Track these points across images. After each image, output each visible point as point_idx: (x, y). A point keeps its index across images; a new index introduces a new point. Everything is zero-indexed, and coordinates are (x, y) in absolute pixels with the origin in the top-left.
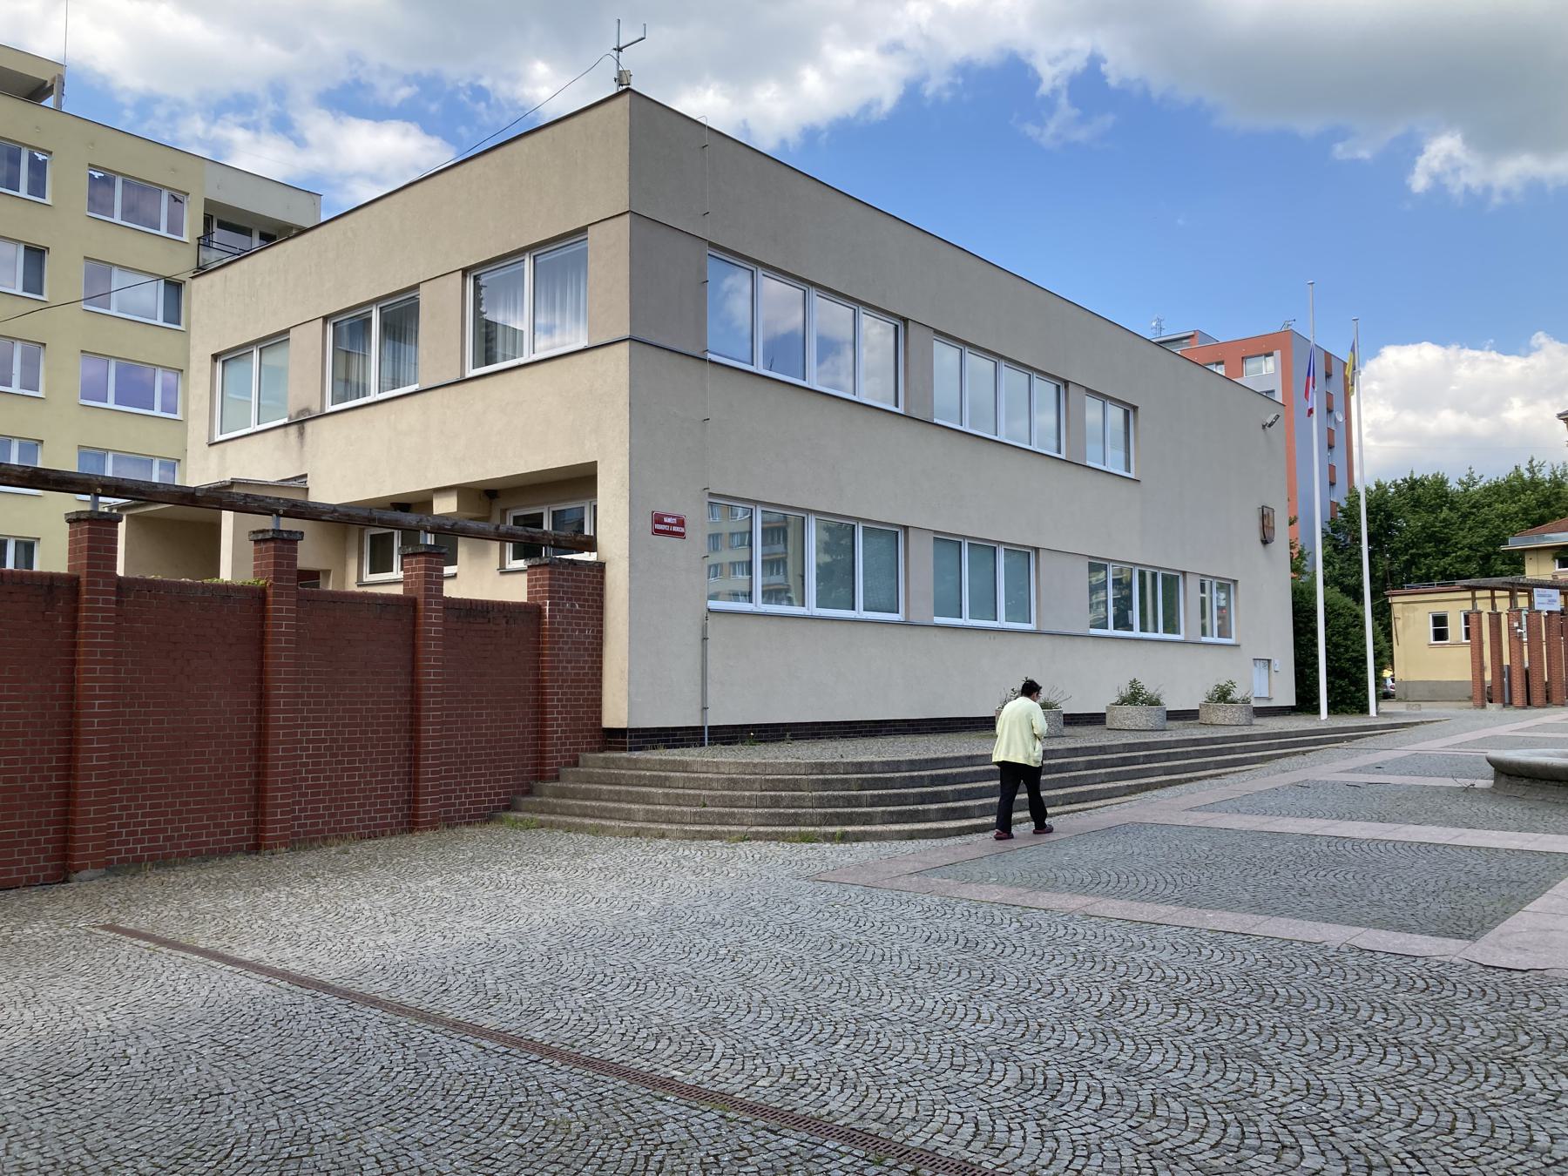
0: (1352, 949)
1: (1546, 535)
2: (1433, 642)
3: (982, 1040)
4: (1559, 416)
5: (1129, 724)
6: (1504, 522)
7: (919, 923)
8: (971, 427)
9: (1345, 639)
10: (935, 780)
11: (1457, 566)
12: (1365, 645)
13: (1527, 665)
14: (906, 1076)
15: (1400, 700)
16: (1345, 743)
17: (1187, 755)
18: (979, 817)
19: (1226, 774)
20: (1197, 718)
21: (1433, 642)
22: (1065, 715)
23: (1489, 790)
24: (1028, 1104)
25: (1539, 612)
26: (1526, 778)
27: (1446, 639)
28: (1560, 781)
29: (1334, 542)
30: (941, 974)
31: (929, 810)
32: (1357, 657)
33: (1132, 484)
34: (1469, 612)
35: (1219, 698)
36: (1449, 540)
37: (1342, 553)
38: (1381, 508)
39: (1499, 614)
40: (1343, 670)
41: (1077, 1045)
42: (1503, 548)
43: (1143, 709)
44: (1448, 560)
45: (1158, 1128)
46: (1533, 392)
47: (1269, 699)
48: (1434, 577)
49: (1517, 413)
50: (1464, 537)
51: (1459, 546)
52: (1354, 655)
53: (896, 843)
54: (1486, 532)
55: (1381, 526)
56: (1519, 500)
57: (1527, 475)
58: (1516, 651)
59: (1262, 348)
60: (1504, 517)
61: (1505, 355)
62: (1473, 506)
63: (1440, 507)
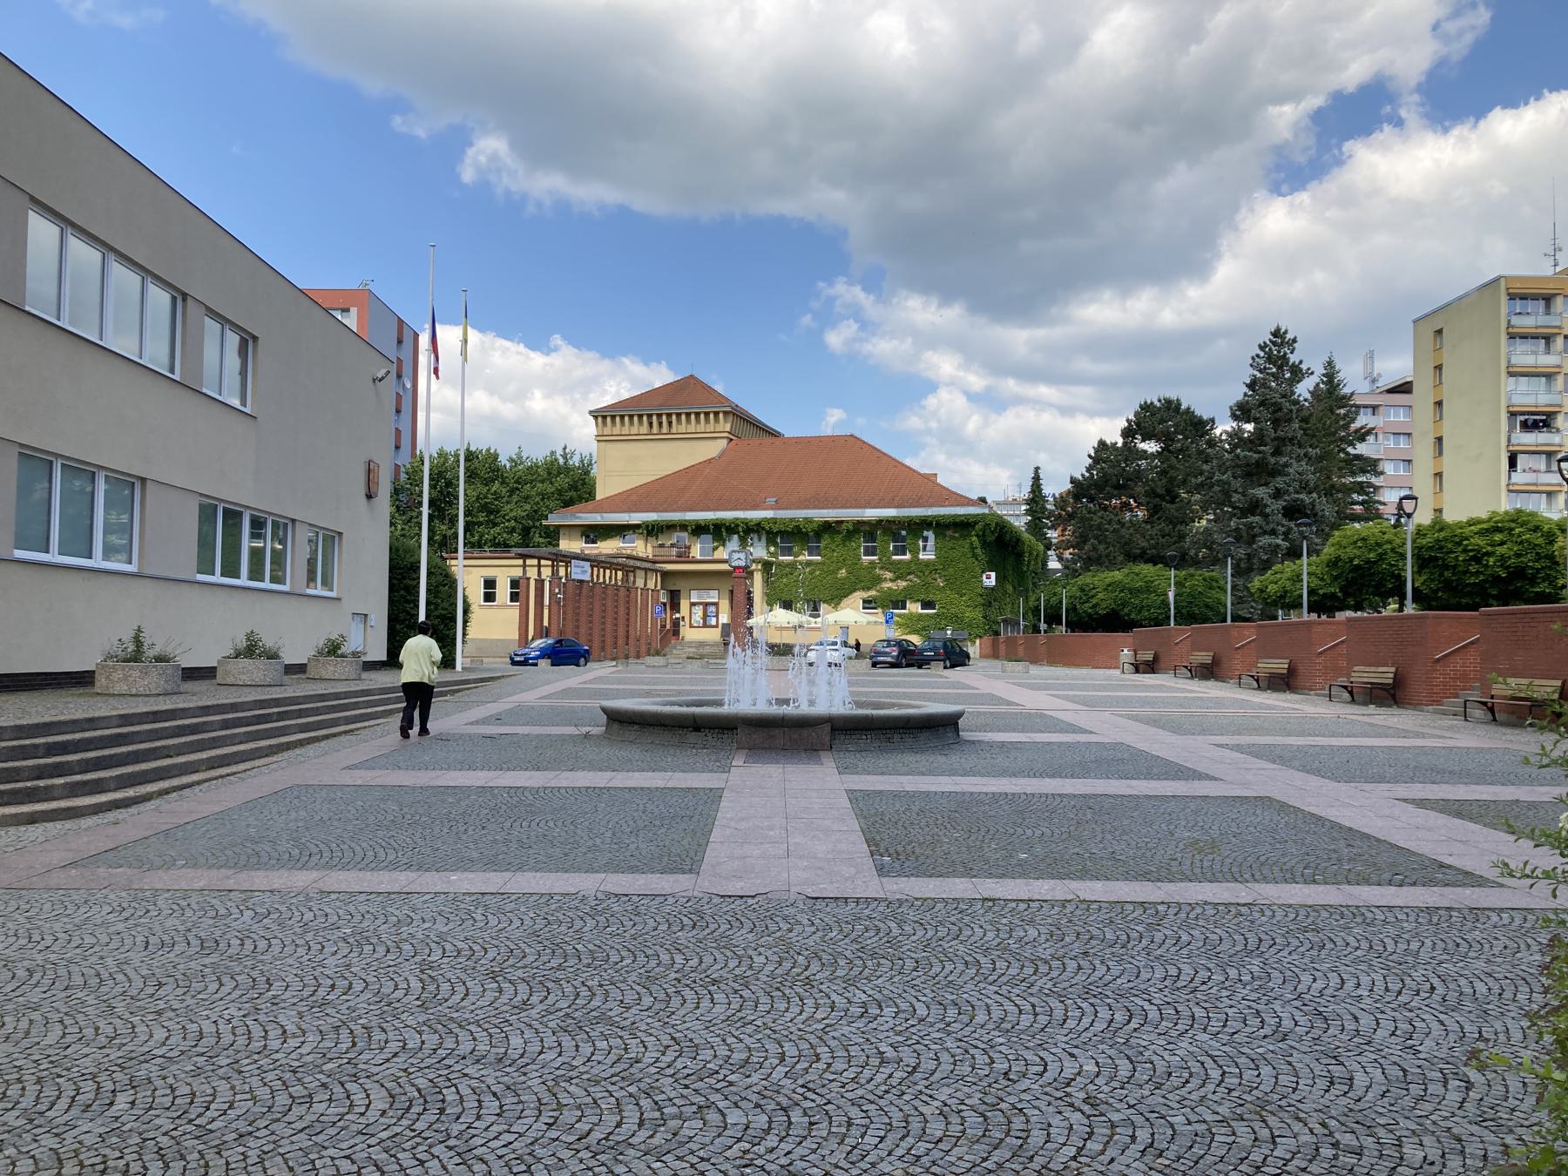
0: (608, 895)
1: (578, 515)
2: (483, 603)
3: (309, 1059)
4: (591, 412)
5: (245, 679)
6: (543, 499)
7: (120, 927)
8: (71, 323)
10: (52, 750)
13: (546, 623)
14: (242, 1126)
17: (316, 712)
18: (115, 790)
20: (305, 672)
21: (483, 603)
22: (183, 669)
24: (420, 1126)
27: (494, 601)
29: (397, 503)
30: (197, 986)
31: (53, 786)
32: (444, 615)
36: (498, 512)
37: (404, 514)
38: (443, 479)
39: (543, 581)
41: (423, 1042)
42: (544, 522)
43: (261, 663)
44: (498, 529)
45: (575, 1119)
46: (554, 388)
49: (538, 403)
50: (511, 510)
53: (12, 830)
54: (528, 507)
55: (440, 492)
57: (561, 461)
60: (543, 496)
62: (517, 482)
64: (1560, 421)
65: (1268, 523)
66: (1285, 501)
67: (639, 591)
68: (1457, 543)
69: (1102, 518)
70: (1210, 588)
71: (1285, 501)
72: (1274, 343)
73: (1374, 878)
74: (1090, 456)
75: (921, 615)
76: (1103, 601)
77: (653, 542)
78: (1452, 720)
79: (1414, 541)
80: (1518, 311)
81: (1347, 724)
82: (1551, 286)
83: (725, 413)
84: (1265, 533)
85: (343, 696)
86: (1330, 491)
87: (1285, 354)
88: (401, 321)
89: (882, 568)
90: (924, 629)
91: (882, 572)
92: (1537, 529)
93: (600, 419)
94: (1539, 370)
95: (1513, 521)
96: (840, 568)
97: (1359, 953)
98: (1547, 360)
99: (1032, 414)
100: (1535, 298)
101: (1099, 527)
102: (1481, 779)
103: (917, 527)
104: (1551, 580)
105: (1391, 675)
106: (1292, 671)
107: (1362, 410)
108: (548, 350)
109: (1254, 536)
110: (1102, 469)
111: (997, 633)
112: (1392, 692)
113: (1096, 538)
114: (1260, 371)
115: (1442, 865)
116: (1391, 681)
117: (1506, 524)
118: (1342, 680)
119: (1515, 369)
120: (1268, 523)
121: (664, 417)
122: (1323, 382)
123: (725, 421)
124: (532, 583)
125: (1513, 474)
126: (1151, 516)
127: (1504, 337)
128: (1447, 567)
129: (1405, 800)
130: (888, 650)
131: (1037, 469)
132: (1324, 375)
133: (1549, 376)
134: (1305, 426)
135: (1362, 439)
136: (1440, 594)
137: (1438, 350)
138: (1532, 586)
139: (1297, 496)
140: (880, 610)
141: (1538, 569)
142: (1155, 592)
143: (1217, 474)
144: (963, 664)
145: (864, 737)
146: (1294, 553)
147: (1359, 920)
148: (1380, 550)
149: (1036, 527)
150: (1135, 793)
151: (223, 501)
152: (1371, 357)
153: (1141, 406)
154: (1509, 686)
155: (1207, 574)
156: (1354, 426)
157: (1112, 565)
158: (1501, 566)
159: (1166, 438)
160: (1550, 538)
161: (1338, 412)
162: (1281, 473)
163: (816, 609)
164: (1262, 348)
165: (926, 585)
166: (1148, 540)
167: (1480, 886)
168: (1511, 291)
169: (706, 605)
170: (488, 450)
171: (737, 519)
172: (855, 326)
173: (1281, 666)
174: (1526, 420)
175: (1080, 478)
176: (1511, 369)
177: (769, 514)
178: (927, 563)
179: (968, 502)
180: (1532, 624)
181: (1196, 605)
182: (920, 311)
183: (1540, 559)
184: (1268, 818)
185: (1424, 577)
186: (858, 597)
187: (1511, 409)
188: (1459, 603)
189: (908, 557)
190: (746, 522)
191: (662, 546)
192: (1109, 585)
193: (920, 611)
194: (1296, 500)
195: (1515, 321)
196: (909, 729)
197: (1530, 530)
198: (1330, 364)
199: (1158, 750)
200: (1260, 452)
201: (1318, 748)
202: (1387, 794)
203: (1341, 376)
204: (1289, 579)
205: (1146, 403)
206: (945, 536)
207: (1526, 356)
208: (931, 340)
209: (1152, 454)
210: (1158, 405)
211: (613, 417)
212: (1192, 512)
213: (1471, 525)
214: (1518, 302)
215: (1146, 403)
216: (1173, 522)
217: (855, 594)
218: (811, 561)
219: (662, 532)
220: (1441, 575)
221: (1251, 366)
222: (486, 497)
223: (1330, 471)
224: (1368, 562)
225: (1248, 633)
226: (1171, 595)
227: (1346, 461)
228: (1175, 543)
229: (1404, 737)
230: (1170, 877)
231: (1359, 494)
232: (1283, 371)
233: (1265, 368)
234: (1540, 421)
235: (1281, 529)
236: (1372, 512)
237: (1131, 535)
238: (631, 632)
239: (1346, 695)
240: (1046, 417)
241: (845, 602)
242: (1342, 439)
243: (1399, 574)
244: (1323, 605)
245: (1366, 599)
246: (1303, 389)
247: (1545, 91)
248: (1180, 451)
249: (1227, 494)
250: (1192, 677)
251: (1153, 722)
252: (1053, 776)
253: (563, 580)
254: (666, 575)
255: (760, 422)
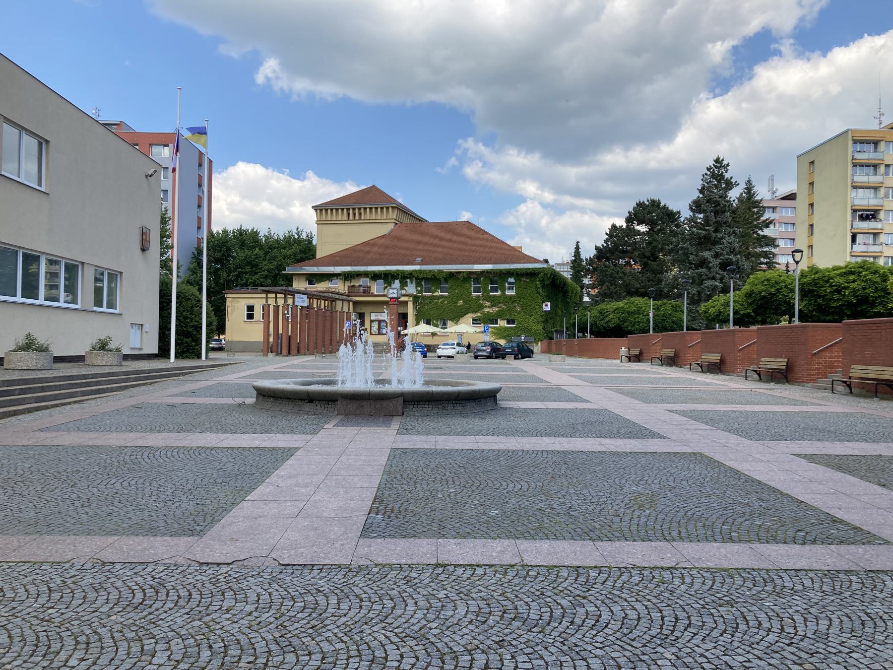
1: (304, 268)
2: (246, 320)
4: (313, 207)
9: (190, 314)
11: (261, 280)
12: (202, 319)
13: (290, 334)
15: (227, 351)
16: (181, 377)
17: (60, 387)
19: (88, 399)
21: (246, 320)
23: (253, 406)
25: (297, 306)
26: (272, 397)
28: (290, 399)
33: (42, 195)
34: (264, 305)
35: (100, 348)
39: (279, 306)
40: (188, 332)
42: (284, 272)
43: (32, 354)
44: (257, 276)
47: (141, 349)
48: (249, 285)
51: (263, 269)
52: (196, 323)
56: (292, 248)
57: (296, 236)
58: (285, 327)
59: (163, 140)
61: (293, 178)
63: (255, 247)
64: (882, 215)
65: (710, 273)
66: (721, 259)
67: (338, 312)
68: (826, 281)
69: (613, 270)
70: (676, 311)
71: (721, 259)
72: (716, 167)
73: (780, 536)
74: (607, 234)
75: (507, 327)
76: (613, 319)
77: (348, 284)
78: (824, 392)
79: (799, 280)
80: (858, 150)
81: (757, 395)
82: (878, 135)
83: (393, 208)
84: (709, 278)
85: (90, 377)
86: (748, 256)
87: (722, 173)
88: (201, 154)
89: (483, 300)
90: (508, 336)
91: (484, 302)
92: (876, 272)
93: (318, 211)
94: (870, 185)
95: (861, 267)
96: (459, 300)
97: (772, 638)
98: (874, 179)
99: (579, 215)
100: (868, 142)
101: (611, 276)
102: (851, 437)
103: (502, 276)
104: (884, 304)
105: (785, 364)
106: (722, 361)
107: (767, 210)
108: (303, 179)
109: (702, 281)
110: (614, 241)
111: (551, 338)
112: (785, 374)
113: (609, 282)
114: (707, 183)
115: (836, 521)
116: (785, 367)
117: (857, 269)
118: (754, 367)
119: (856, 184)
120: (710, 273)
121: (357, 210)
122: (745, 193)
123: (393, 212)
124: (272, 308)
125: (854, 246)
126: (643, 269)
127: (850, 166)
128: (820, 296)
129: (799, 456)
130: (484, 348)
131: (578, 243)
132: (745, 188)
133: (876, 188)
134: (733, 216)
135: (767, 226)
136: (814, 313)
137: (811, 173)
138: (872, 309)
139: (728, 256)
140: (482, 325)
141: (876, 297)
142: (643, 313)
143: (681, 243)
144: (529, 357)
145: (427, 406)
146: (725, 290)
147: (769, 588)
148: (778, 287)
149: (577, 277)
150: (604, 449)
151: (22, 248)
152: (773, 179)
153: (637, 204)
154: (858, 371)
155: (674, 303)
156: (762, 219)
157: (619, 298)
158: (853, 295)
159: (651, 223)
160: (884, 278)
161: (753, 210)
162: (719, 243)
163: (445, 324)
164: (708, 169)
165: (510, 310)
166: (640, 283)
167: (869, 542)
168: (855, 138)
169: (380, 321)
170: (253, 229)
171: (398, 270)
172: (480, 164)
173: (716, 358)
174: (862, 214)
175: (601, 247)
176: (854, 184)
177: (417, 268)
178: (511, 297)
179: (536, 261)
180: (877, 331)
181: (667, 322)
182: (516, 158)
183: (877, 291)
184: (698, 472)
185: (805, 303)
186: (469, 317)
187: (854, 208)
188: (825, 319)
189: (499, 293)
190: (403, 272)
191: (353, 286)
192: (616, 309)
193: (506, 325)
194: (727, 259)
195: (857, 156)
196: (459, 400)
197: (872, 273)
198: (749, 182)
199: (630, 415)
200: (706, 230)
201: (737, 413)
202: (786, 450)
203: (755, 189)
204: (722, 305)
205: (640, 202)
206: (521, 281)
207: (862, 177)
208: (521, 174)
209: (643, 232)
210: (647, 203)
211: (326, 210)
212: (666, 267)
213: (834, 270)
214: (858, 145)
215: (640, 202)
216: (654, 272)
217: (468, 315)
218: (442, 295)
219: (354, 279)
220: (816, 301)
221: (702, 180)
222: (250, 257)
223: (749, 245)
224: (770, 294)
225: (696, 338)
226: (651, 315)
227: (757, 239)
228: (656, 285)
229: (795, 405)
230: (609, 535)
231: (764, 258)
232: (721, 183)
233: (710, 181)
234: (870, 215)
235: (718, 276)
236: (771, 265)
237: (630, 280)
238: (334, 338)
239: (756, 376)
240: (586, 218)
241: (462, 320)
242: (755, 226)
243: (790, 301)
244: (742, 321)
245: (769, 317)
246: (734, 194)
247: (866, 35)
248: (659, 231)
249: (686, 255)
250: (662, 365)
251: (632, 394)
252: (548, 435)
253: (316, 309)
254: (356, 303)
255: (415, 214)
